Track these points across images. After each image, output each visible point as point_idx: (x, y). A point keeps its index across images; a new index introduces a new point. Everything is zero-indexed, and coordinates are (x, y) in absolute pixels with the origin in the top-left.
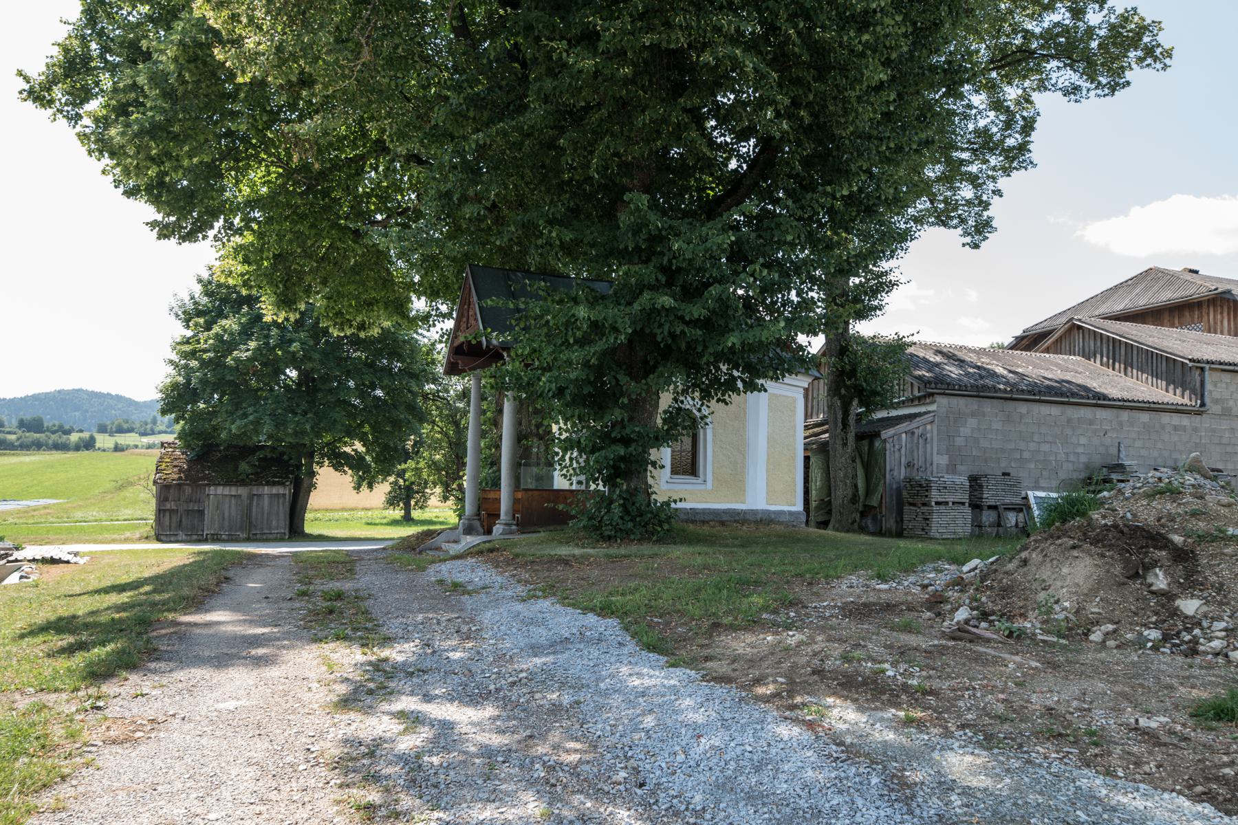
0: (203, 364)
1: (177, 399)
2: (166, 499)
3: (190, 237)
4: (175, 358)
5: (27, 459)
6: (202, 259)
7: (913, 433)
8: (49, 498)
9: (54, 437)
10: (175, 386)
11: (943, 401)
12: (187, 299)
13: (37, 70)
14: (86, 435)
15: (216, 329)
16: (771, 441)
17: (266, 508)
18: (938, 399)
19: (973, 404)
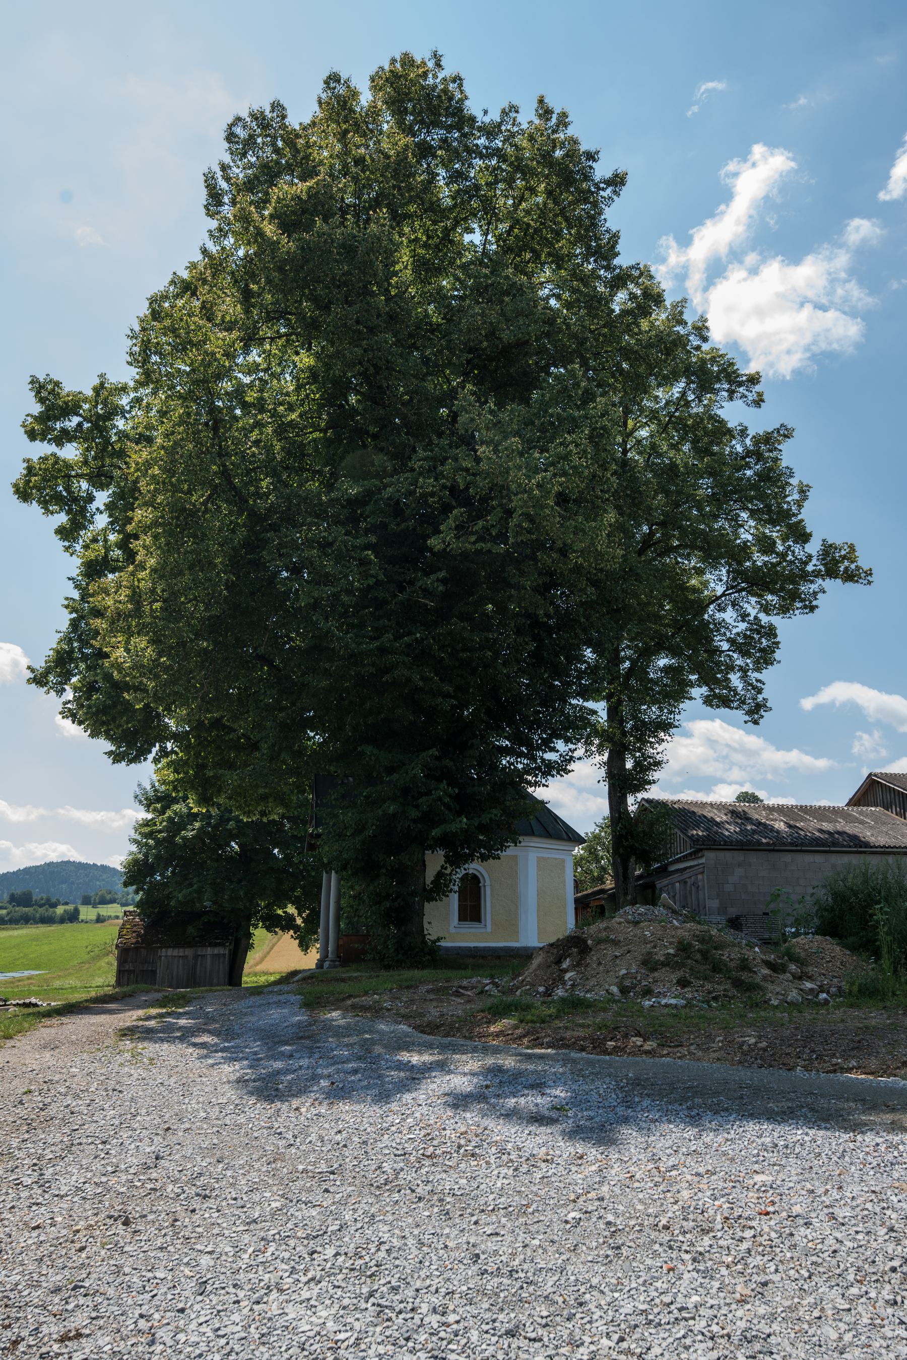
0: (158, 842)
1: (137, 872)
2: (125, 961)
3: (135, 760)
4: (139, 837)
5: (15, 933)
6: (147, 773)
7: (686, 882)
8: (33, 969)
9: (41, 910)
10: (135, 862)
11: (710, 855)
12: (148, 787)
13: (40, 664)
14: (71, 907)
15: (169, 813)
16: (541, 893)
17: (208, 967)
18: (706, 853)
19: (739, 856)
